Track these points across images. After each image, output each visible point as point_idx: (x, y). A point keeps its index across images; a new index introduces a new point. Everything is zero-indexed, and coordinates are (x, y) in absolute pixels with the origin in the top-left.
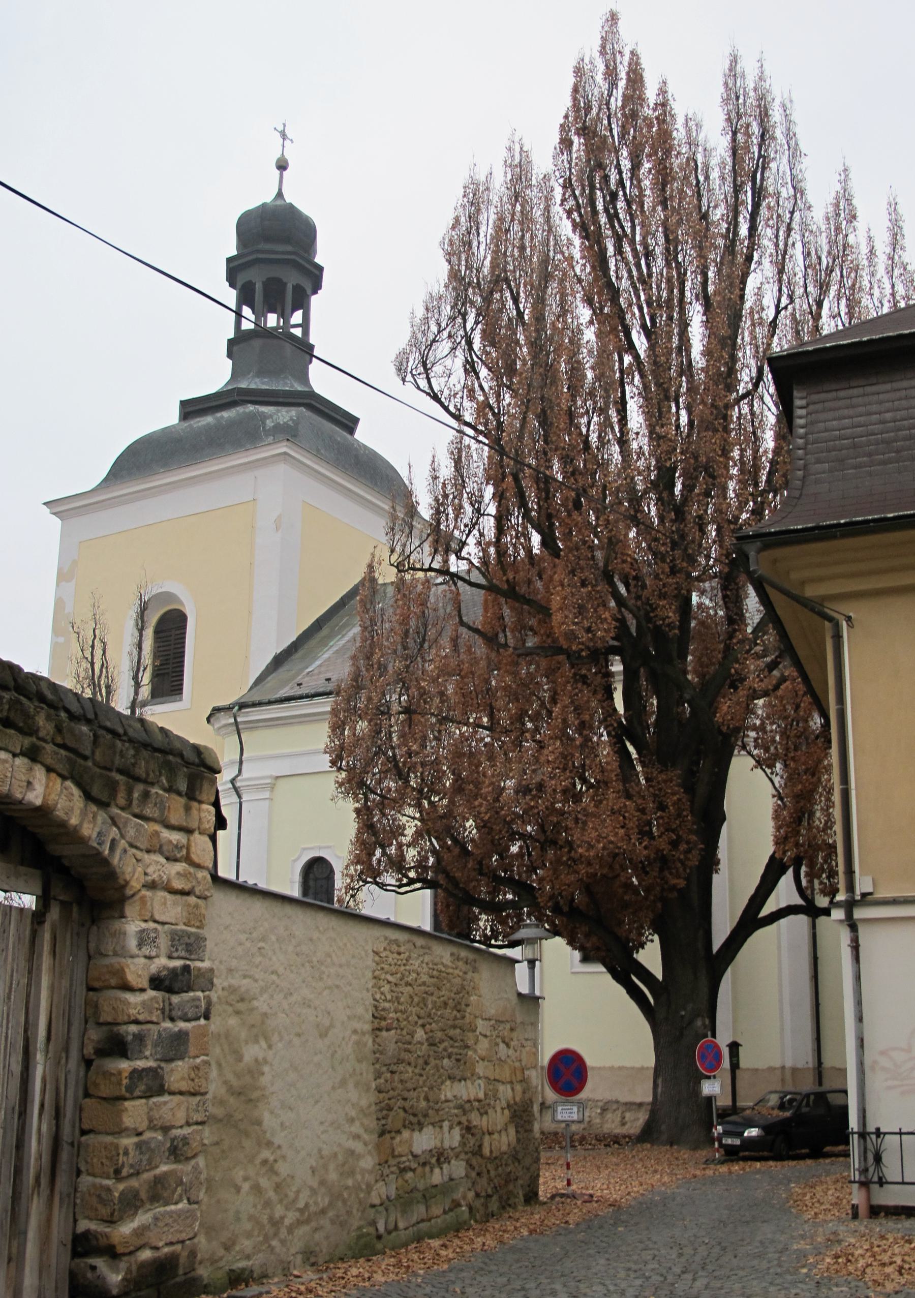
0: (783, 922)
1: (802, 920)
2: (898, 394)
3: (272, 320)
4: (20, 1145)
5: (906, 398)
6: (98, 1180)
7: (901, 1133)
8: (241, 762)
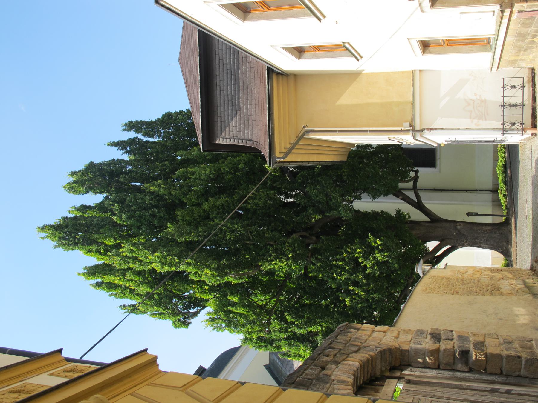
4: (511, 172)
5: (224, 101)
6: (523, 366)
7: (504, 96)
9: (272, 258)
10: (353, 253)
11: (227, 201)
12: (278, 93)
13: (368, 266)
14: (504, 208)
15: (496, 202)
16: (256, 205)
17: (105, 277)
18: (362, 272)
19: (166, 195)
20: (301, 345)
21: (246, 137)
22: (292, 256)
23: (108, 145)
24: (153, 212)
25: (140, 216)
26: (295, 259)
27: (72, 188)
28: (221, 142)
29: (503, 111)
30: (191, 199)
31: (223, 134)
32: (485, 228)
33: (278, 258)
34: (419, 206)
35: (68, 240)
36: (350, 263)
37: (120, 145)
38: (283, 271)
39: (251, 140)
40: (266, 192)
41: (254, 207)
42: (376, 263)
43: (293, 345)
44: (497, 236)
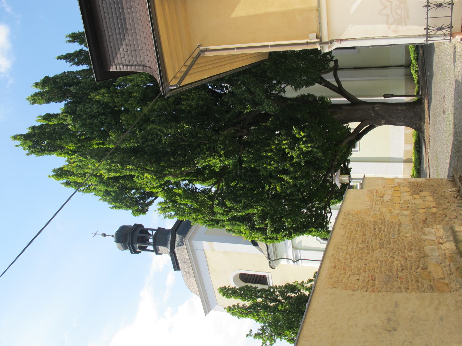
0: (340, 79)
1: (339, 73)
2: (109, 28)
3: (151, 240)
5: (110, 24)
7: (428, 18)
8: (287, 259)
9: (206, 155)
10: (280, 144)
11: (163, 104)
12: (164, 10)
13: (294, 156)
14: (416, 82)
15: (409, 76)
16: (189, 106)
17: (70, 177)
18: (289, 161)
19: (110, 102)
20: (242, 224)
21: (139, 63)
22: (224, 153)
23: (58, 59)
24: (101, 119)
25: (91, 124)
26: (227, 155)
27: (37, 98)
28: (115, 70)
29: (427, 13)
30: (132, 104)
31: (116, 60)
32: (401, 108)
33: (212, 156)
34: (340, 91)
35: (36, 147)
36: (278, 154)
37: (68, 57)
38: (217, 167)
39: (144, 66)
40: (198, 93)
41: (188, 108)
42: (302, 153)
43: (235, 224)
44: (412, 115)
